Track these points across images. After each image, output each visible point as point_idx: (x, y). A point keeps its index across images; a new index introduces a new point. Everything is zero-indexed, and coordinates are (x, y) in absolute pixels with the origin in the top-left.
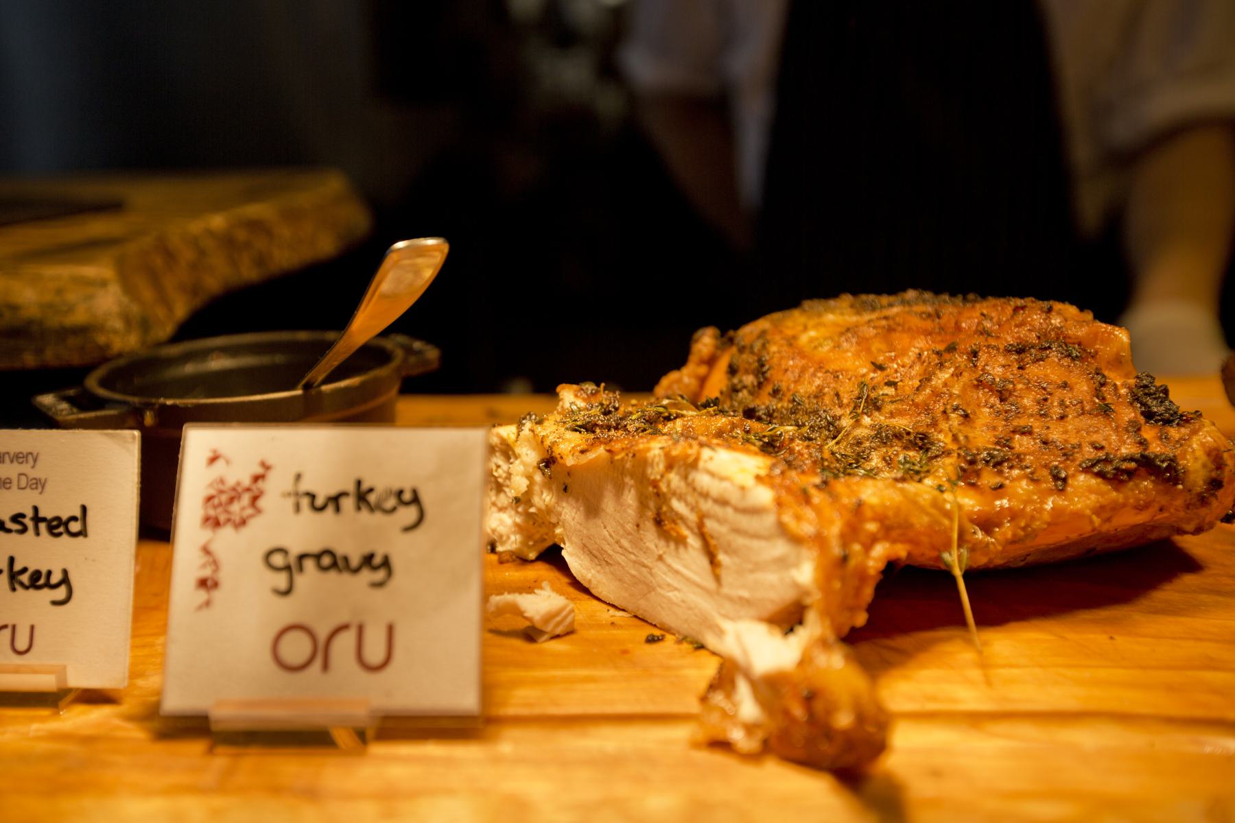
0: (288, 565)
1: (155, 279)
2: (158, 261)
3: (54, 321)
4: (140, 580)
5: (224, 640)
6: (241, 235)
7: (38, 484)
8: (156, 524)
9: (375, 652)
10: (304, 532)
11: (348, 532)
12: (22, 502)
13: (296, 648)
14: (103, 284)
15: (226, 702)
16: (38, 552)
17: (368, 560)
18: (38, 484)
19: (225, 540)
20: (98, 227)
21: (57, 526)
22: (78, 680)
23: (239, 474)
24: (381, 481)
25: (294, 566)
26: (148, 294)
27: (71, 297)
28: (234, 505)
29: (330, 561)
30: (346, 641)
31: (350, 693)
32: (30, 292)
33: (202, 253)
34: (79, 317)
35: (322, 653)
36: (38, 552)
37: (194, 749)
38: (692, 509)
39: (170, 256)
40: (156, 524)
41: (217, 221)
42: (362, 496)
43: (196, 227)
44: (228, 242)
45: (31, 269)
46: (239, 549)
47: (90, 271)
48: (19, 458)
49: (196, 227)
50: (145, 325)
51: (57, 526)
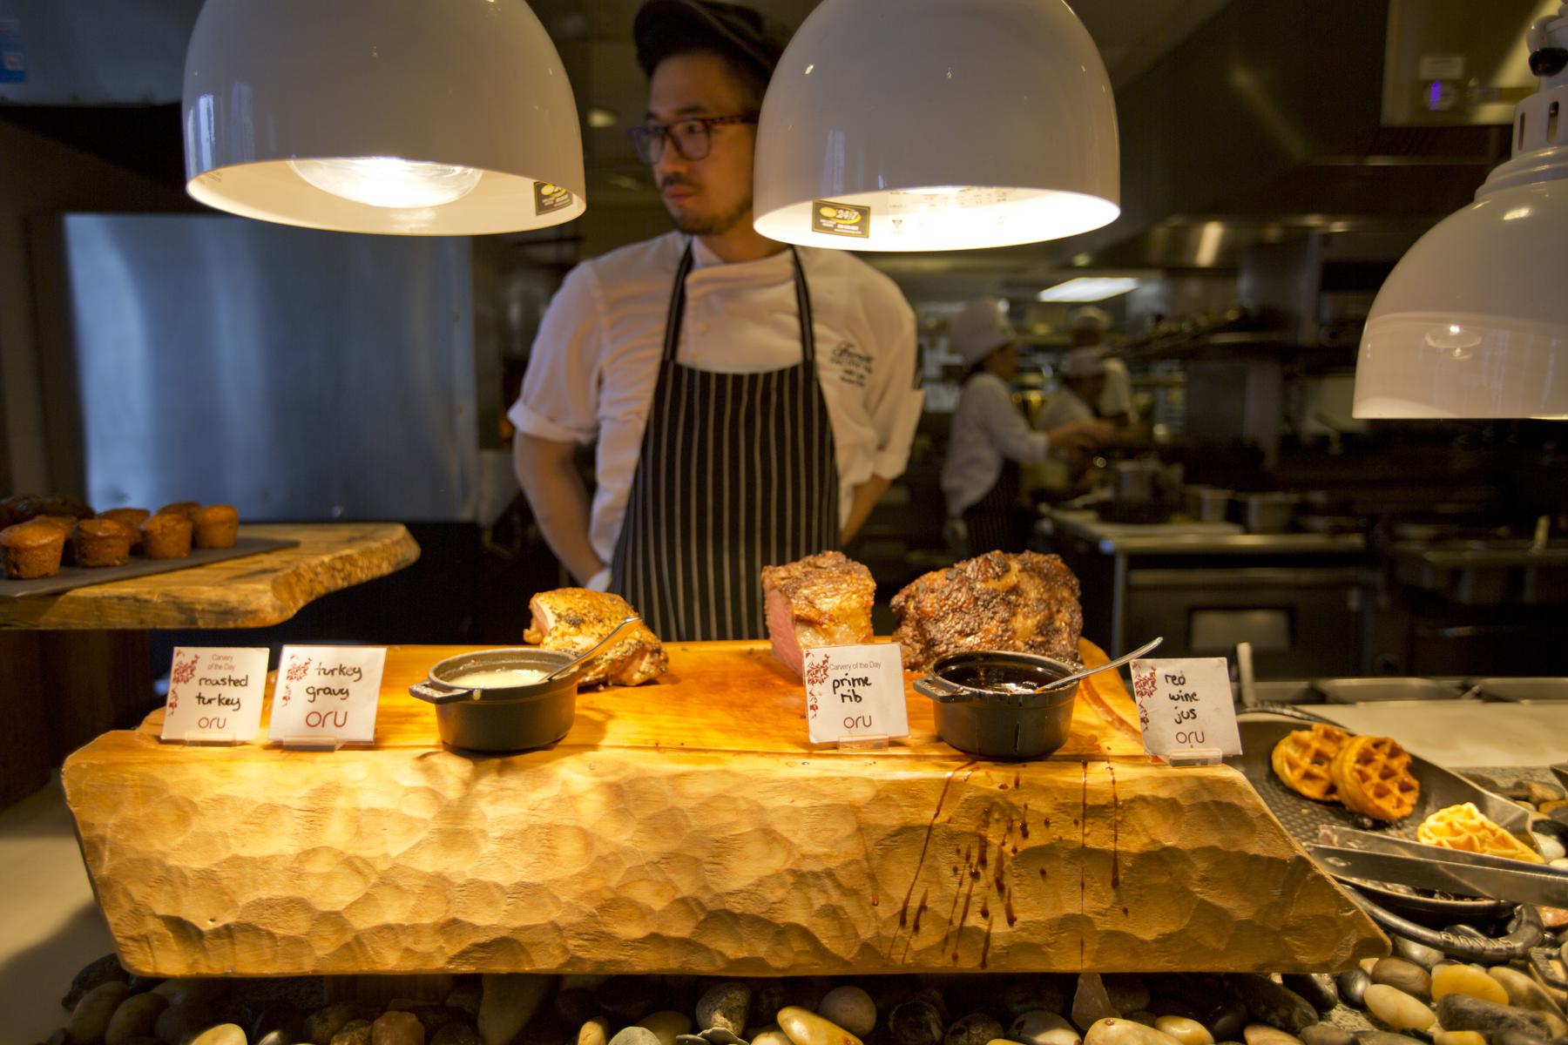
0: (314, 693)
1: (290, 587)
2: (293, 580)
3: (242, 608)
4: (265, 706)
5: (290, 719)
6: (339, 565)
7: (231, 668)
8: (270, 687)
9: (340, 721)
10: (318, 681)
11: (335, 682)
12: (225, 674)
13: (314, 719)
14: (265, 592)
15: (287, 737)
16: (229, 692)
17: (341, 691)
18: (231, 668)
19: (294, 684)
20: (269, 560)
21: (236, 683)
22: (239, 738)
23: (300, 662)
24: (348, 665)
25: (316, 693)
26: (285, 595)
27: (251, 598)
28: (297, 673)
29: (328, 691)
30: (331, 717)
31: (329, 734)
32: (1562, 912)
33: (317, 574)
34: (254, 606)
35: (322, 721)
36: (229, 692)
37: (277, 752)
38: (1425, 998)
39: (298, 575)
40: (270, 687)
41: (326, 559)
42: (341, 670)
43: (315, 561)
44: (331, 568)
45: (236, 585)
46: (299, 689)
47: (260, 587)
48: (226, 658)
49: (315, 561)
50: (282, 610)
51: (236, 683)
